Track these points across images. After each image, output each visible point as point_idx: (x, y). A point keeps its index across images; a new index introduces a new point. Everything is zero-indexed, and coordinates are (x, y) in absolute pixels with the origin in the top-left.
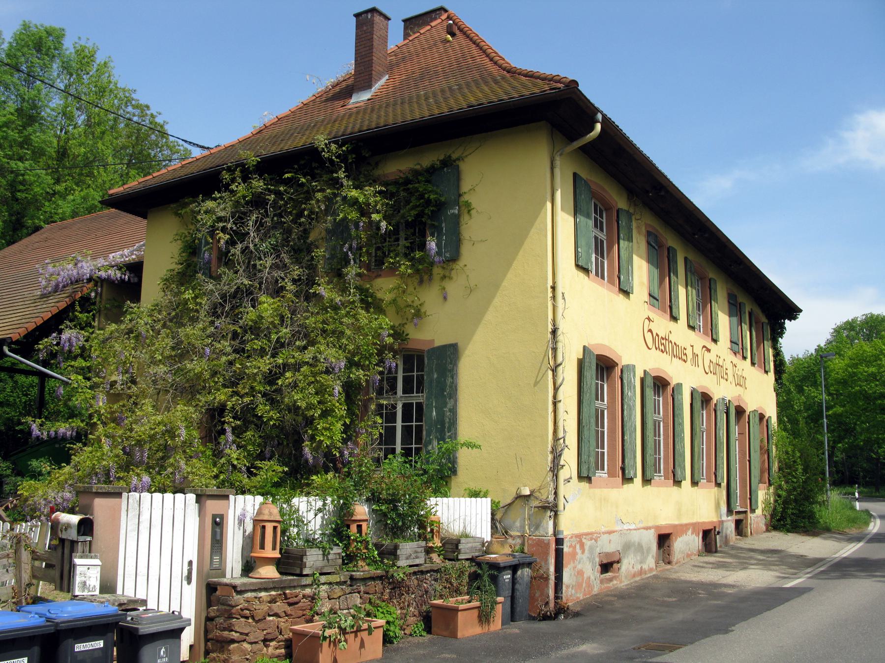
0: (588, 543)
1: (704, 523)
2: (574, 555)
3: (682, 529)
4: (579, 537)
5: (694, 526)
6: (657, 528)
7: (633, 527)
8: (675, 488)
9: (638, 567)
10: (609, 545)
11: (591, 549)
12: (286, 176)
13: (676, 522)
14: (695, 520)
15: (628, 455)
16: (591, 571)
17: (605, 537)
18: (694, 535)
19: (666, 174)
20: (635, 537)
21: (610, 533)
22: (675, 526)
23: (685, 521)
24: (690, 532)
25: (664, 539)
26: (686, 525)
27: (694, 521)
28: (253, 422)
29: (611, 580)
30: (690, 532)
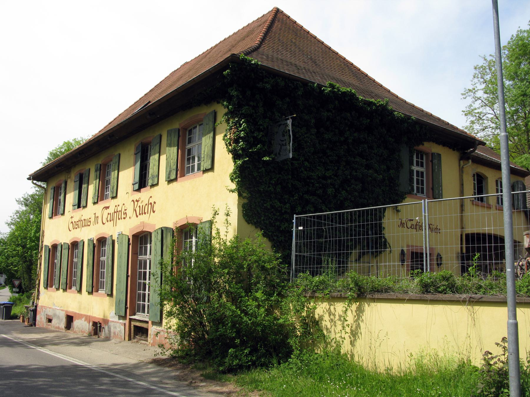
0: (44, 310)
1: (95, 318)
2: (40, 312)
3: (80, 316)
4: (42, 306)
5: (88, 318)
6: (66, 311)
7: (58, 308)
8: (79, 294)
9: (57, 325)
10: (50, 313)
11: (45, 312)
12: (265, 159)
13: (77, 312)
14: (89, 314)
15: (91, 262)
16: (44, 320)
17: (48, 309)
18: (86, 322)
19: (306, 27)
20: (58, 312)
21: (50, 308)
22: (75, 313)
23: (83, 312)
24: (83, 319)
25: (70, 319)
26: (82, 315)
27: (89, 314)
28: (479, 108)
29: (49, 325)
30: (83, 319)
